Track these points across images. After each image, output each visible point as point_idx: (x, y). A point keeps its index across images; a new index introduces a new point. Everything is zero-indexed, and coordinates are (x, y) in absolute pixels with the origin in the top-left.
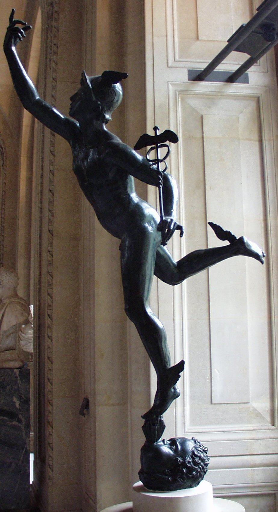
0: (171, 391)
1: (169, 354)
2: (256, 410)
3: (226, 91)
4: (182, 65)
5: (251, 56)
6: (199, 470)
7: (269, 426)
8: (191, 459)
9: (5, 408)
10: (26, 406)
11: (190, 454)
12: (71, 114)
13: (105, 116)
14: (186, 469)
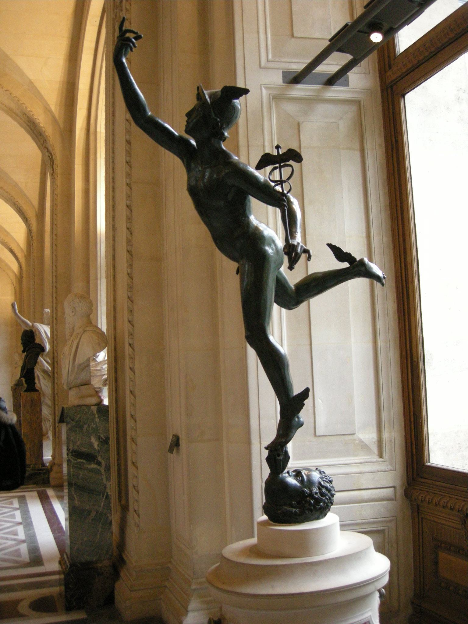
0: (295, 420)
1: (292, 381)
2: (363, 442)
3: (325, 95)
4: (276, 65)
5: (354, 56)
6: (326, 501)
7: (376, 458)
8: (318, 490)
9: (83, 449)
10: (106, 446)
11: (317, 485)
12: (187, 132)
13: (223, 134)
14: (313, 500)
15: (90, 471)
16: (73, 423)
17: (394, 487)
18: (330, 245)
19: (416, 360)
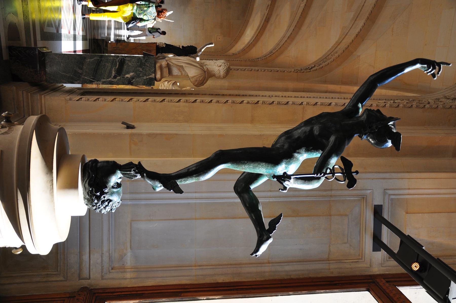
4: (387, 201)
6: (98, 205)
9: (125, 67)
10: (127, 83)
15: (110, 71)
16: (143, 61)
17: (89, 278)
18: (281, 215)
19: (182, 295)
